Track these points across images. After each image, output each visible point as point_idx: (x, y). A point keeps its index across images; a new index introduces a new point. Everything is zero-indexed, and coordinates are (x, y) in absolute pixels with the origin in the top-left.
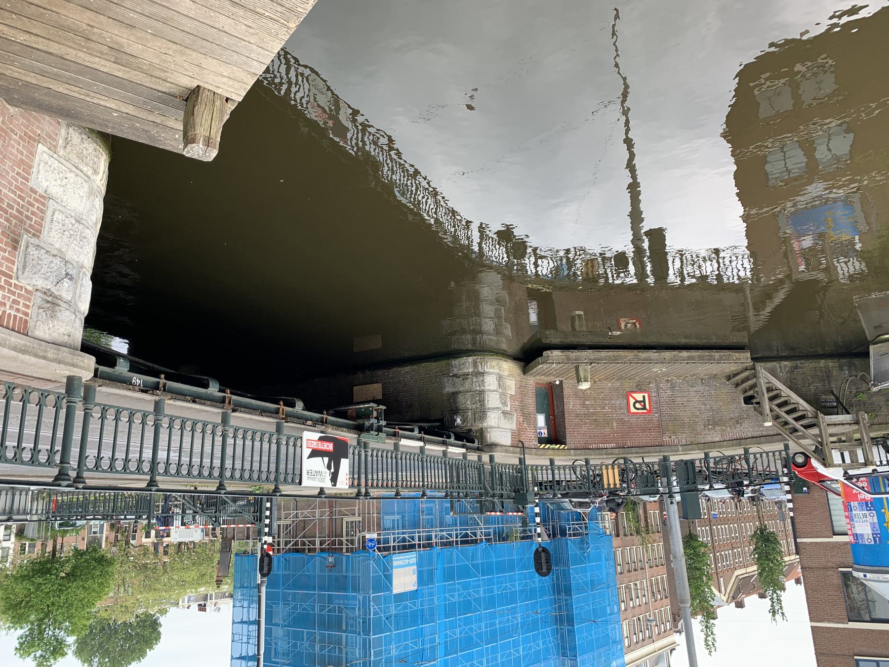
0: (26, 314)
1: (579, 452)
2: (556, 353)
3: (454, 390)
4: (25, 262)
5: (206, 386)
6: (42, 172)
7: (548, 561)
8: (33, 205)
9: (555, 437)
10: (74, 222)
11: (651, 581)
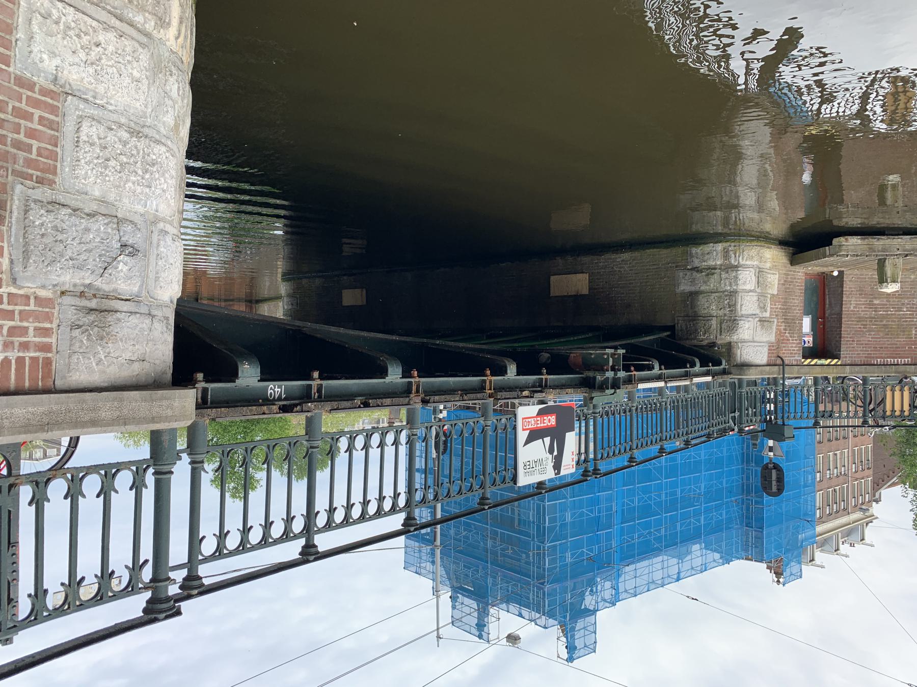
0: (46, 348)
1: (857, 368)
2: (854, 241)
3: (693, 289)
4: (26, 244)
5: (383, 373)
6: (38, 38)
7: (780, 480)
8: (28, 117)
9: (824, 347)
10: (125, 135)
11: (853, 451)
